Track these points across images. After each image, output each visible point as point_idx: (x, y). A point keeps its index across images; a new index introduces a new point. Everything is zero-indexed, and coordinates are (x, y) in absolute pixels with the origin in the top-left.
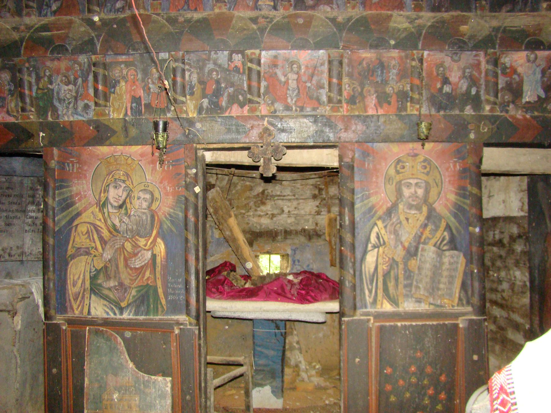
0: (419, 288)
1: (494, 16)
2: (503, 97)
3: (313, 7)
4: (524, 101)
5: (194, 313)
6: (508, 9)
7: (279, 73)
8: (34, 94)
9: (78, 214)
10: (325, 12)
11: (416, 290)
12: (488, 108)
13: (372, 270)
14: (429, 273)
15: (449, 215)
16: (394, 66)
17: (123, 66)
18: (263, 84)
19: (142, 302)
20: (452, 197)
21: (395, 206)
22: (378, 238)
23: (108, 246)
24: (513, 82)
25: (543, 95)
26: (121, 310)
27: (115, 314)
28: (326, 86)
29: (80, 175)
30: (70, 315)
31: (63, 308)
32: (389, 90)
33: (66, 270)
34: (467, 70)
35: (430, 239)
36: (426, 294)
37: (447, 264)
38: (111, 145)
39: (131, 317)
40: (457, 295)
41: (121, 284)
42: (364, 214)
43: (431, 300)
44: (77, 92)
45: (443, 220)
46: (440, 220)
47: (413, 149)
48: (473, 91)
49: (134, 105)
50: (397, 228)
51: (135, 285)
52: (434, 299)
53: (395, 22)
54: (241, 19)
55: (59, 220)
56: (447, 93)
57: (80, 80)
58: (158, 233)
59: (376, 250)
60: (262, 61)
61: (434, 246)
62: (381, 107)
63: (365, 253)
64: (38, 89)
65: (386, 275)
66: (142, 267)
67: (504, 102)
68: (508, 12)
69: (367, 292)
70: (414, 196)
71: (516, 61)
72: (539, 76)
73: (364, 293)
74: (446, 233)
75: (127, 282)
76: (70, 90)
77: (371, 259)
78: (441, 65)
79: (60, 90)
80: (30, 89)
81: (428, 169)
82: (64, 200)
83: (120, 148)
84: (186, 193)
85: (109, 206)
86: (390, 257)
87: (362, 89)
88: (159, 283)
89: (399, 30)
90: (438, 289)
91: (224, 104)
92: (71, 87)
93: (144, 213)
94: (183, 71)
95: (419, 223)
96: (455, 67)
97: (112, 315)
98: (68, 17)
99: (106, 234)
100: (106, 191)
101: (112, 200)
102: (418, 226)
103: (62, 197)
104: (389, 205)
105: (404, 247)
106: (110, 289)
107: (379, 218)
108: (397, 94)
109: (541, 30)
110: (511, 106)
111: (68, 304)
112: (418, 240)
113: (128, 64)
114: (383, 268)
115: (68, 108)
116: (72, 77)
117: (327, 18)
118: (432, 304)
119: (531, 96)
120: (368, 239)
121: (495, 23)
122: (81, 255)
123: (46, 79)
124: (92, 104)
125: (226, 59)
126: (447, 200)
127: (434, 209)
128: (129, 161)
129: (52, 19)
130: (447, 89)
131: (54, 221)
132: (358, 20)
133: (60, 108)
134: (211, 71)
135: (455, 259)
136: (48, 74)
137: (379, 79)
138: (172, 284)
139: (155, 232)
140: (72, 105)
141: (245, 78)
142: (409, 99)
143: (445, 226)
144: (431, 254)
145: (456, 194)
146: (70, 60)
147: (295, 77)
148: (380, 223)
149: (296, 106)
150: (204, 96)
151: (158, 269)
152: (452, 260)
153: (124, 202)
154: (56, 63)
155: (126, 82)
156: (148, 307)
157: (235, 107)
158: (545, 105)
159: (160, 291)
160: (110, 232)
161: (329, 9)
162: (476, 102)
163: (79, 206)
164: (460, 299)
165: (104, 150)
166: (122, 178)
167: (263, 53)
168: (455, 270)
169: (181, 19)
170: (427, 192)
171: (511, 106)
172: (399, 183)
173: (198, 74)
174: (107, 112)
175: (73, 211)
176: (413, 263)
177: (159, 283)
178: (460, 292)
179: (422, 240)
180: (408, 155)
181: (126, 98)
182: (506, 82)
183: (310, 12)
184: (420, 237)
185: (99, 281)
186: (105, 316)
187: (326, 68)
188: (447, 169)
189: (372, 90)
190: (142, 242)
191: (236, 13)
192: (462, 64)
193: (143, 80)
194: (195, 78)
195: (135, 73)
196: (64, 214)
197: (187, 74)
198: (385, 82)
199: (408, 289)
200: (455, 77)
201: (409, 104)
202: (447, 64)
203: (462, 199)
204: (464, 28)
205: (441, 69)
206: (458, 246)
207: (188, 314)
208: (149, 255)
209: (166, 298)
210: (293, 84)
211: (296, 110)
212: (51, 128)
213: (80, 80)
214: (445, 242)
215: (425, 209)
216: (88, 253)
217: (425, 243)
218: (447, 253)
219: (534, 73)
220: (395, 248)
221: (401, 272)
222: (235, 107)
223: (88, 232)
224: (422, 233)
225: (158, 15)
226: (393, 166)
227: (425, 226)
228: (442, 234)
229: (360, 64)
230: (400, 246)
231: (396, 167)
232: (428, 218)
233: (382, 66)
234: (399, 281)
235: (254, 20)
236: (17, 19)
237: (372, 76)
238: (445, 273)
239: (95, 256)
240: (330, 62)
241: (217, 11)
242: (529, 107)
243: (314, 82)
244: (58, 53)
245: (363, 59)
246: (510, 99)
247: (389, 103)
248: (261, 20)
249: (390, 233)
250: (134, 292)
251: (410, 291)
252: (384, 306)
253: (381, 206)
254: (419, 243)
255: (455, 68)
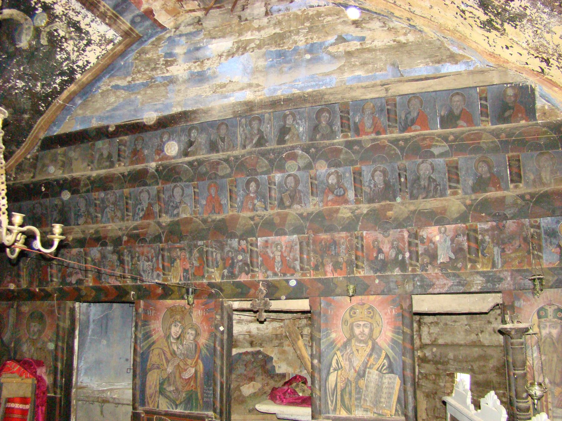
0: (366, 401)
1: (412, 203)
2: (423, 260)
3: (289, 207)
4: (439, 262)
5: (218, 411)
6: (424, 196)
7: (269, 251)
8: (130, 268)
9: (154, 343)
10: (297, 209)
11: (364, 402)
12: (410, 269)
13: (333, 386)
14: (374, 390)
15: (387, 347)
16: (343, 243)
17: (178, 250)
18: (260, 259)
19: (189, 402)
20: (390, 334)
21: (349, 340)
22: (338, 364)
23: (170, 364)
24: (430, 249)
25: (453, 256)
26: (177, 406)
27: (173, 409)
28: (299, 259)
29: (156, 318)
30: (147, 408)
31: (143, 403)
32: (340, 260)
33: (146, 378)
34: (395, 243)
35: (373, 365)
36: (372, 406)
37: (387, 383)
38: (171, 299)
39: (182, 411)
40: (394, 407)
41: (177, 389)
42: (328, 346)
43: (375, 410)
44: (153, 266)
45: (383, 351)
46: (381, 352)
47: (362, 300)
48: (400, 257)
49: (185, 274)
50: (350, 356)
51: (185, 390)
52: (377, 409)
53: (342, 213)
54: (244, 217)
55: (143, 346)
56: (381, 260)
57: (154, 260)
58: (199, 357)
59: (336, 372)
60: (259, 244)
61: (377, 370)
62: (336, 271)
63: (328, 374)
64: (132, 264)
65: (343, 391)
66: (189, 379)
67: (424, 263)
68: (424, 198)
69: (330, 402)
70: (362, 333)
71: (431, 233)
72: (449, 243)
73: (328, 403)
74: (385, 361)
75: (180, 388)
76: (149, 265)
77: (332, 378)
78: (376, 240)
79: (143, 265)
80: (128, 265)
81: (372, 314)
82: (147, 333)
83: (178, 301)
84: (215, 331)
85: (172, 338)
86: (346, 377)
87: (323, 259)
88: (199, 390)
89: (344, 218)
90: (380, 402)
91: (236, 273)
92: (150, 263)
93: (191, 343)
94: (212, 252)
95: (366, 353)
96: (386, 240)
97: (171, 410)
98: (148, 221)
99: (169, 355)
100: (170, 328)
101: (173, 334)
102: (366, 355)
103: (145, 331)
104: (345, 340)
105: (355, 370)
106: (170, 392)
107: (338, 349)
108: (346, 262)
109: (446, 210)
110: (429, 266)
111: (146, 400)
112: (365, 365)
113: (181, 249)
114: (340, 385)
115: (148, 276)
116: (150, 257)
117: (297, 214)
118: (375, 413)
119: (444, 258)
120: (330, 365)
121: (412, 208)
122: (154, 369)
123: (136, 258)
124: (161, 273)
125: (237, 244)
126: (386, 336)
127: (377, 343)
128: (183, 309)
129: (139, 222)
130: (381, 257)
131: (140, 347)
132: (317, 214)
133: (144, 276)
134: (229, 251)
135: (393, 380)
136: (137, 255)
137: (333, 253)
138: (206, 390)
139: (197, 356)
140: (150, 274)
141: (248, 255)
142: (354, 265)
143: (384, 356)
144: (374, 376)
145: (394, 332)
146: (149, 247)
147: (279, 253)
148: (338, 353)
149: (281, 273)
150: (225, 268)
151: (199, 380)
152: (390, 381)
153: (180, 335)
154: (141, 249)
155: (180, 260)
156: (192, 404)
157: (243, 275)
158: (455, 265)
159: (199, 395)
160: (171, 354)
161: (299, 207)
162: (403, 265)
163: (155, 337)
164: (396, 410)
165: (169, 302)
166: (179, 320)
167: (259, 239)
168: (393, 388)
169: (210, 220)
170: (372, 330)
171: (429, 266)
172: (352, 325)
173: (221, 253)
174: (169, 279)
175: (151, 340)
176: (362, 383)
177: (199, 390)
178: (396, 405)
179: (368, 366)
180: (358, 304)
181: (180, 269)
182: (425, 249)
183: (287, 210)
184: (367, 363)
185: (164, 387)
186: (167, 409)
187: (298, 247)
188: (386, 314)
189: (329, 260)
190: (189, 362)
191: (241, 214)
192: (390, 238)
193: (190, 259)
194: (219, 256)
195: (184, 254)
196: (146, 342)
197: (214, 254)
198: (337, 255)
199: (358, 401)
200: (387, 248)
201: (355, 269)
202: (380, 239)
203: (397, 336)
204: (390, 213)
205: (376, 243)
206: (395, 371)
207: (215, 411)
208: (193, 370)
209: (203, 399)
210: (278, 259)
211: (281, 276)
212: (138, 289)
213: (154, 260)
214: (385, 367)
215: (370, 343)
216: (158, 368)
217: (370, 368)
218: (387, 376)
219: (445, 241)
220: (349, 371)
221: (353, 388)
222: (243, 275)
223: (159, 354)
224: (368, 361)
225: (197, 217)
226: (348, 311)
227: (370, 355)
228: (383, 361)
229: (321, 242)
230: (353, 370)
231: (350, 313)
232: (373, 349)
233: (335, 243)
234: (352, 394)
235: (252, 218)
236: (122, 223)
237: (328, 251)
238: (385, 391)
239: (163, 370)
240: (301, 243)
241: (231, 213)
242: (443, 267)
243: (291, 257)
244: (142, 243)
245: (322, 240)
246: (428, 261)
247: (341, 269)
248: (256, 218)
249: (346, 360)
250: (184, 395)
251: (360, 403)
252: (341, 413)
253: (340, 341)
254: (366, 368)
255: (386, 241)
